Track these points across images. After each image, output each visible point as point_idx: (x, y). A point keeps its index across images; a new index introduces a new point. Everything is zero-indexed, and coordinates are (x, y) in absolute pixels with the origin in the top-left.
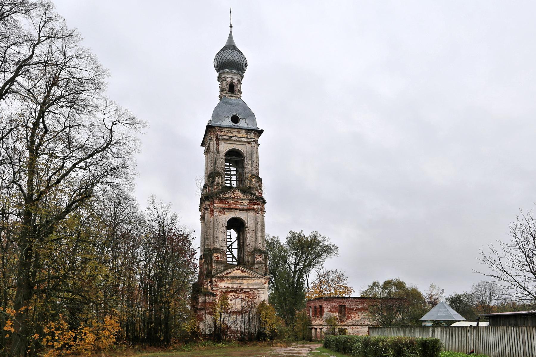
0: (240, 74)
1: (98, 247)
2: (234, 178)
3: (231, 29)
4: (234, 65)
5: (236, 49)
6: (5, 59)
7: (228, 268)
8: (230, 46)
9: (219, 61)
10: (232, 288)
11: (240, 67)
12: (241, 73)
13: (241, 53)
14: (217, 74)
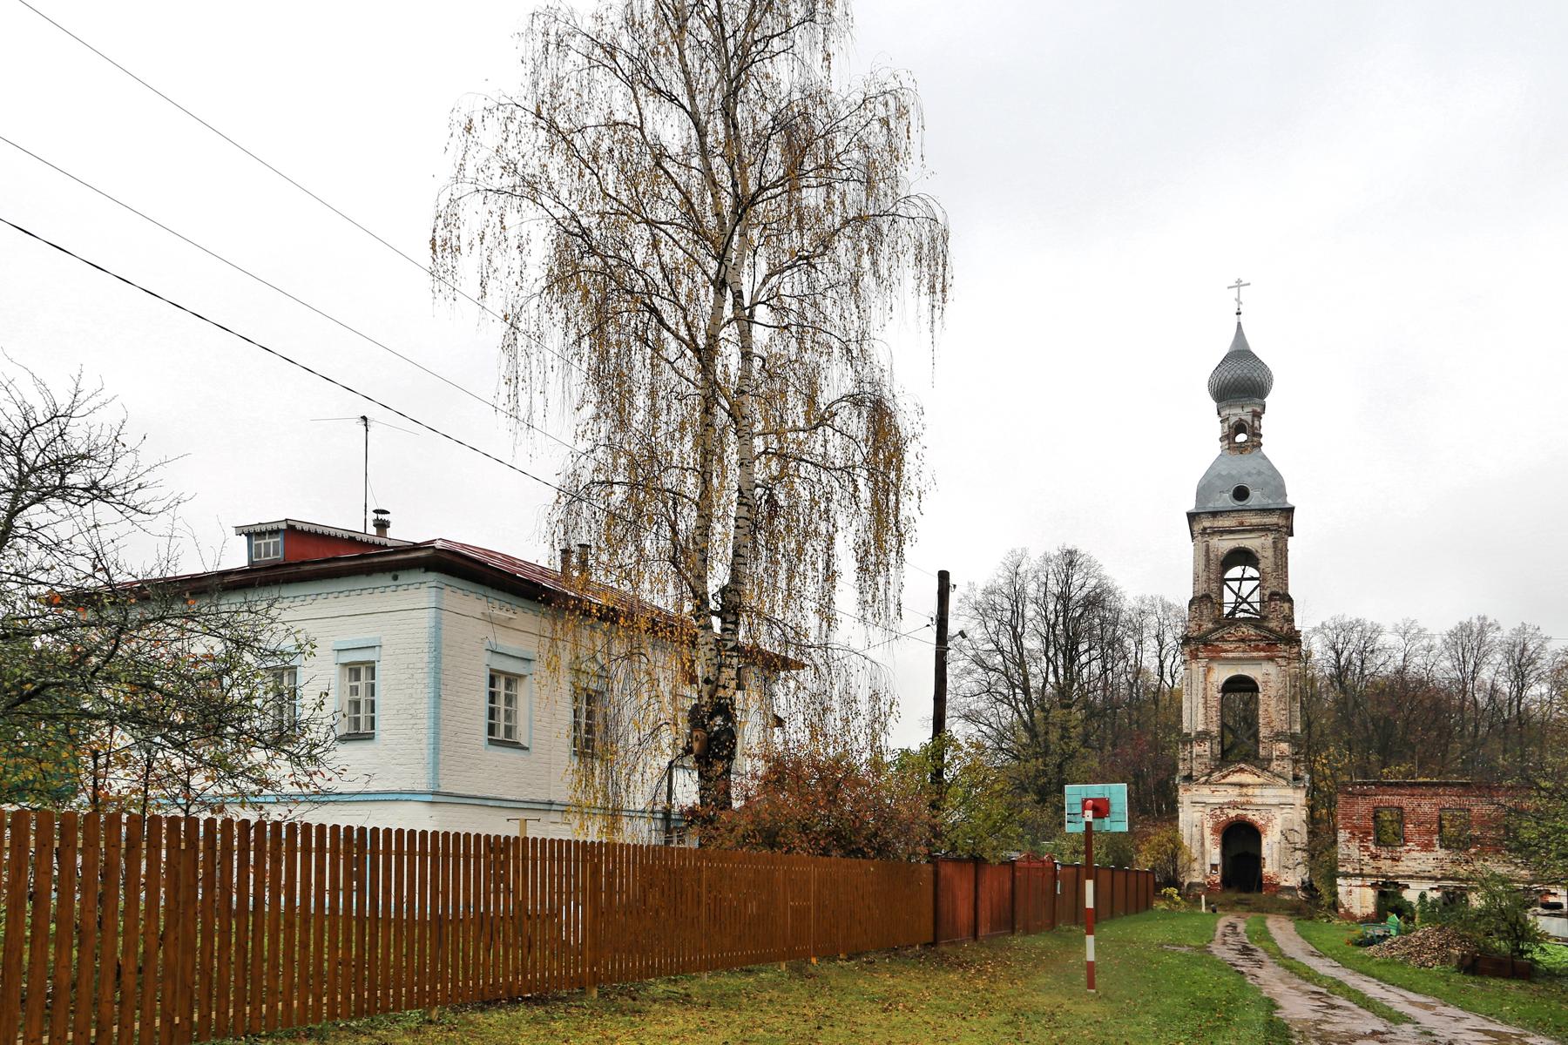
3: (1239, 319)
8: (1240, 353)
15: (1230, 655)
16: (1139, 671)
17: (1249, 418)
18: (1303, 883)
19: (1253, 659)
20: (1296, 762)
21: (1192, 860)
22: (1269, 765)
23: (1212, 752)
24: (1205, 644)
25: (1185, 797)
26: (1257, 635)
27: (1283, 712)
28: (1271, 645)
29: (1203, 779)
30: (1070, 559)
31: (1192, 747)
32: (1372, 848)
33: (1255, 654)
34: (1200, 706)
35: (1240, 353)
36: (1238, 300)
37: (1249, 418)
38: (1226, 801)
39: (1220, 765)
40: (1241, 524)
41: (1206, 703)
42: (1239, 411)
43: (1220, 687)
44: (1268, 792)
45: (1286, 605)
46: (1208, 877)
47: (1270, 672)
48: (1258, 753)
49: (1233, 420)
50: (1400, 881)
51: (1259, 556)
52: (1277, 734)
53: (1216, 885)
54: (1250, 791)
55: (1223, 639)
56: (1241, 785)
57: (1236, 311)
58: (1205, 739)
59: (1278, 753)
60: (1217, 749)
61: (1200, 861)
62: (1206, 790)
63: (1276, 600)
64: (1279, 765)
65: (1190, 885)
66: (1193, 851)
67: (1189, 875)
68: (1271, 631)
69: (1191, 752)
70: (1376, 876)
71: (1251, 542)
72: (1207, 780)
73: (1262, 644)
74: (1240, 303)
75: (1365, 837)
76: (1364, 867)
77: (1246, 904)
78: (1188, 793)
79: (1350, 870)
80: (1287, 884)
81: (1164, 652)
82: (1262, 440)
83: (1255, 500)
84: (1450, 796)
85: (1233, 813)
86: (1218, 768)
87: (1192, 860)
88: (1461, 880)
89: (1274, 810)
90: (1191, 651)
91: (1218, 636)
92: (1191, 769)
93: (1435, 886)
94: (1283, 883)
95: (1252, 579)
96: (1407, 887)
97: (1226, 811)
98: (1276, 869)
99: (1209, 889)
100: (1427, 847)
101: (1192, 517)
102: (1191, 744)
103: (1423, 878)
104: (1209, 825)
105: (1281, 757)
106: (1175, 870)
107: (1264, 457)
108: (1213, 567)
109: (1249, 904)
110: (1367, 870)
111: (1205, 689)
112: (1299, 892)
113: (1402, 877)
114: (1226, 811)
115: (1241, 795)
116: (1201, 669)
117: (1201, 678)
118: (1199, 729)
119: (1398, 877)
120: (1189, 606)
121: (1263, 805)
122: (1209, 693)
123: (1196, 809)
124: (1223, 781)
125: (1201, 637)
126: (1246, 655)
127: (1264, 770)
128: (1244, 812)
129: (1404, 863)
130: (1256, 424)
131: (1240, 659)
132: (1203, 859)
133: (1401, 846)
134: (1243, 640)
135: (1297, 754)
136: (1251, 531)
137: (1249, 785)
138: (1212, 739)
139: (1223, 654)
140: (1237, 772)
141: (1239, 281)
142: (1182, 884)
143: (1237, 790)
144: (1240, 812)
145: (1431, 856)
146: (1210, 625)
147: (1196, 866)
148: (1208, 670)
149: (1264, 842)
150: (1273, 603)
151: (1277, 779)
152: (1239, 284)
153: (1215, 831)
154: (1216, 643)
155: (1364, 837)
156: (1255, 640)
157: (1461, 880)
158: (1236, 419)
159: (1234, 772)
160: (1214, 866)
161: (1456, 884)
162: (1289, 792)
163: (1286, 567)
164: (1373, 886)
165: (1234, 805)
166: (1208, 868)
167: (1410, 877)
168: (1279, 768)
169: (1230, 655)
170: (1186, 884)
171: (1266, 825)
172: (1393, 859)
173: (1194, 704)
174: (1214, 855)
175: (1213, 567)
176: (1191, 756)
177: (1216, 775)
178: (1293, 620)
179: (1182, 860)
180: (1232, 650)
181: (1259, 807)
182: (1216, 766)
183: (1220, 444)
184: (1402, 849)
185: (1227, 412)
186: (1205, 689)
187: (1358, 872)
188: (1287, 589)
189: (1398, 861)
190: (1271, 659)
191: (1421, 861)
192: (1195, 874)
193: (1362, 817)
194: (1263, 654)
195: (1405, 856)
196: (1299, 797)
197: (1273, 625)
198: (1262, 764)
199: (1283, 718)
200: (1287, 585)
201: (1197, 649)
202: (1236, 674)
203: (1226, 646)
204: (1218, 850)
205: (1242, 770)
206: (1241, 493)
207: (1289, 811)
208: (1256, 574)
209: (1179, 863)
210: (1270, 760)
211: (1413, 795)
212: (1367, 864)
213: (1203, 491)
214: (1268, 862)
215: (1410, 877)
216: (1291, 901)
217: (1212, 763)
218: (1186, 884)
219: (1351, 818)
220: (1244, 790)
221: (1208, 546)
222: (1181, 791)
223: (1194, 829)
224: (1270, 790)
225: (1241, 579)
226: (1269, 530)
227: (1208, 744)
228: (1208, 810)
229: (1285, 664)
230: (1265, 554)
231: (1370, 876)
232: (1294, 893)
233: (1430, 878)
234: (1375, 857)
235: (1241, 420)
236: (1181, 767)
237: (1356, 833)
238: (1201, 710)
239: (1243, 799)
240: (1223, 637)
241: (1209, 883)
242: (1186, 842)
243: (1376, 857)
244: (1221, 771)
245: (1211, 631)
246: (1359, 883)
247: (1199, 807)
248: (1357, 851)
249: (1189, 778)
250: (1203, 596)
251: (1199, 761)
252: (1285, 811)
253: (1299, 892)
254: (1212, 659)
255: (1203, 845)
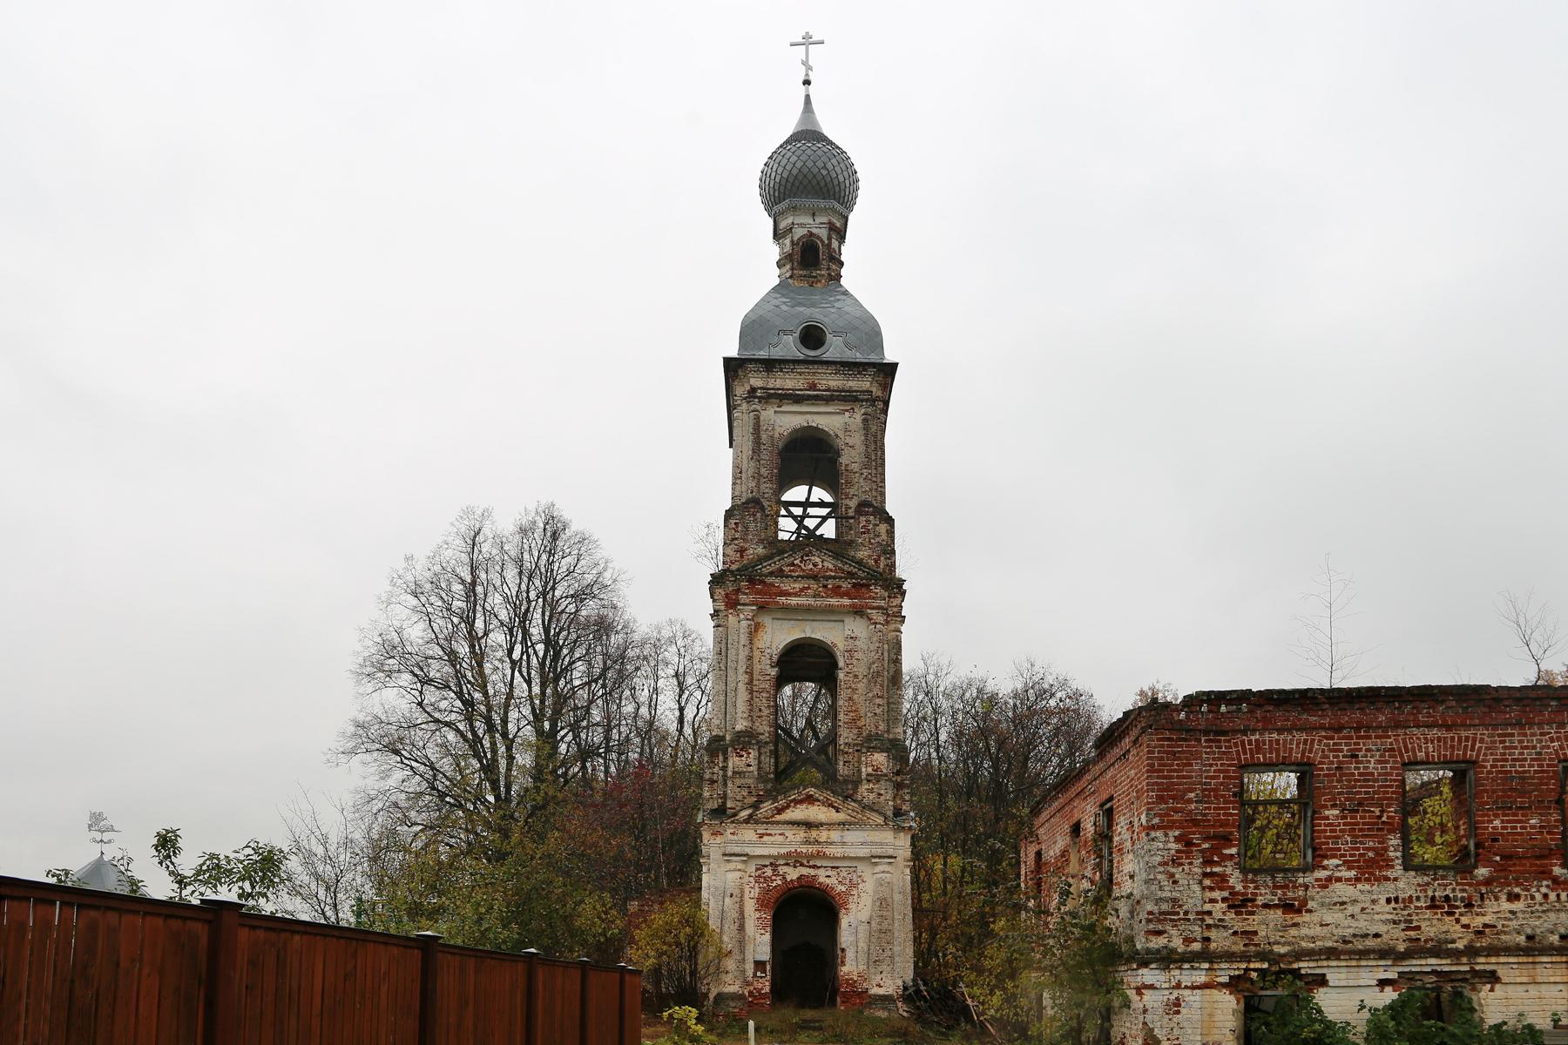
0: (834, 211)
1: (565, 885)
2: (1463, 734)
3: (807, 90)
4: (818, 183)
5: (818, 137)
6: (772, 704)
7: (1286, 769)
8: (808, 136)
9: (773, 177)
10: (521, 643)
11: (837, 189)
12: (837, 205)
13: (831, 143)
14: (769, 223)
15: (794, 601)
16: (649, 730)
17: (823, 233)
18: (905, 988)
19: (830, 610)
20: (899, 786)
21: (723, 954)
22: (855, 790)
23: (759, 768)
24: (752, 581)
25: (712, 845)
26: (837, 569)
27: (878, 701)
28: (860, 588)
29: (744, 814)
30: (554, 531)
31: (726, 759)
32: (1235, 880)
33: (834, 601)
34: (742, 687)
35: (808, 136)
36: (805, 63)
37: (823, 233)
38: (783, 851)
39: (774, 789)
40: (813, 387)
41: (750, 682)
42: (808, 220)
43: (775, 658)
44: (853, 836)
45: (883, 528)
46: (748, 984)
47: (857, 633)
48: (836, 770)
49: (799, 233)
50: (1305, 966)
51: (840, 443)
52: (869, 738)
53: (763, 996)
54: (824, 835)
55: (780, 573)
56: (808, 825)
57: (802, 78)
58: (750, 743)
59: (870, 770)
60: (768, 762)
61: (737, 956)
62: (749, 834)
63: (867, 514)
64: (871, 790)
65: (720, 997)
66: (725, 938)
67: (718, 981)
68: (860, 563)
69: (724, 769)
70: (1245, 957)
71: (830, 420)
72: (750, 816)
73: (846, 585)
74: (810, 68)
75: (1215, 850)
76: (1213, 934)
77: (815, 1029)
78: (719, 839)
79: (1177, 944)
80: (881, 991)
81: (685, 696)
82: (843, 272)
83: (834, 348)
84: (1429, 726)
85: (793, 874)
86: (770, 795)
87: (723, 954)
88: (1456, 954)
89: (861, 867)
90: (727, 595)
91: (774, 568)
92: (724, 797)
93: (1392, 975)
94: (875, 991)
95: (822, 504)
96: (1322, 981)
97: (782, 870)
98: (862, 967)
99: (751, 1004)
100: (1371, 869)
101: (733, 368)
102: (725, 753)
103: (1364, 954)
104: (752, 893)
105: (876, 777)
106: (693, 973)
107: (846, 293)
108: (765, 456)
109: (820, 1029)
110: (1220, 941)
111: (750, 658)
112: (900, 1004)
113: (1310, 954)
114: (782, 870)
115: (807, 842)
116: (744, 624)
117: (744, 639)
118: (739, 727)
119: (1299, 955)
120: (726, 520)
121: (844, 858)
122: (757, 667)
123: (732, 866)
124: (778, 818)
125: (745, 568)
126: (819, 602)
127: (846, 797)
128: (812, 872)
129: (1315, 917)
130: (835, 244)
131: (808, 610)
132: (742, 952)
133: (1306, 869)
134: (815, 577)
135: (898, 773)
136: (828, 400)
137: (822, 824)
138: (760, 744)
139: (782, 600)
140: (801, 802)
141: (807, 37)
142: (706, 995)
143: (801, 834)
144: (805, 871)
145: (1382, 892)
146: (760, 550)
147: (730, 964)
148: (755, 630)
149: (844, 922)
150: (863, 519)
151: (868, 813)
152: (807, 41)
153: (762, 903)
154: (770, 580)
155: (1215, 850)
156: (834, 578)
157: (1456, 954)
158: (804, 231)
159: (797, 802)
160: (759, 965)
161: (1444, 965)
162: (887, 836)
163: (883, 465)
164: (1234, 984)
165: (796, 860)
166: (750, 968)
167: (1331, 953)
168: (872, 796)
169: (794, 601)
170: (712, 996)
171: (848, 893)
172: (1288, 907)
173: (731, 686)
174: (761, 944)
175: (765, 456)
176: (725, 776)
177: (767, 807)
178: (893, 552)
179: (706, 955)
180: (796, 594)
181: (836, 863)
182: (766, 791)
183: (777, 271)
184: (1309, 879)
185: (790, 220)
186: (750, 658)
187: (1196, 946)
188: (883, 501)
189: (1299, 911)
190: (858, 612)
191: (1356, 909)
192: (728, 978)
193: (1207, 794)
194: (846, 601)
195: (1316, 898)
196: (901, 845)
197: (862, 554)
198: (842, 789)
199: (878, 711)
200: (883, 494)
201: (738, 591)
202: (803, 636)
203: (787, 586)
204: (767, 937)
205: (810, 800)
206: (812, 336)
207: (886, 868)
208: (828, 498)
209: (700, 961)
210: (857, 783)
211: (1339, 729)
212: (1220, 925)
213: (751, 329)
214: (850, 954)
215: (1331, 953)
216: (888, 1019)
217: (761, 786)
218: (712, 996)
219: (1179, 798)
220: (814, 833)
221: (757, 418)
222: (706, 836)
223: (727, 900)
224: (857, 833)
225: (806, 504)
226: (856, 400)
227: (754, 753)
228: (751, 868)
229: (881, 619)
230: (850, 441)
231: (1229, 956)
232: (891, 1006)
233: (1385, 953)
234: (1240, 904)
235: (811, 234)
236: (706, 794)
237: (1196, 838)
238: (743, 695)
239: (812, 849)
240: (781, 570)
241: (751, 993)
242: (713, 924)
243: (1245, 902)
244: (775, 800)
245: (761, 560)
246: (1201, 978)
247: (736, 863)
248: (1197, 888)
249: (720, 813)
250: (748, 502)
251: (738, 782)
252: (880, 868)
253: (900, 1004)
254: (762, 608)
255: (742, 928)
